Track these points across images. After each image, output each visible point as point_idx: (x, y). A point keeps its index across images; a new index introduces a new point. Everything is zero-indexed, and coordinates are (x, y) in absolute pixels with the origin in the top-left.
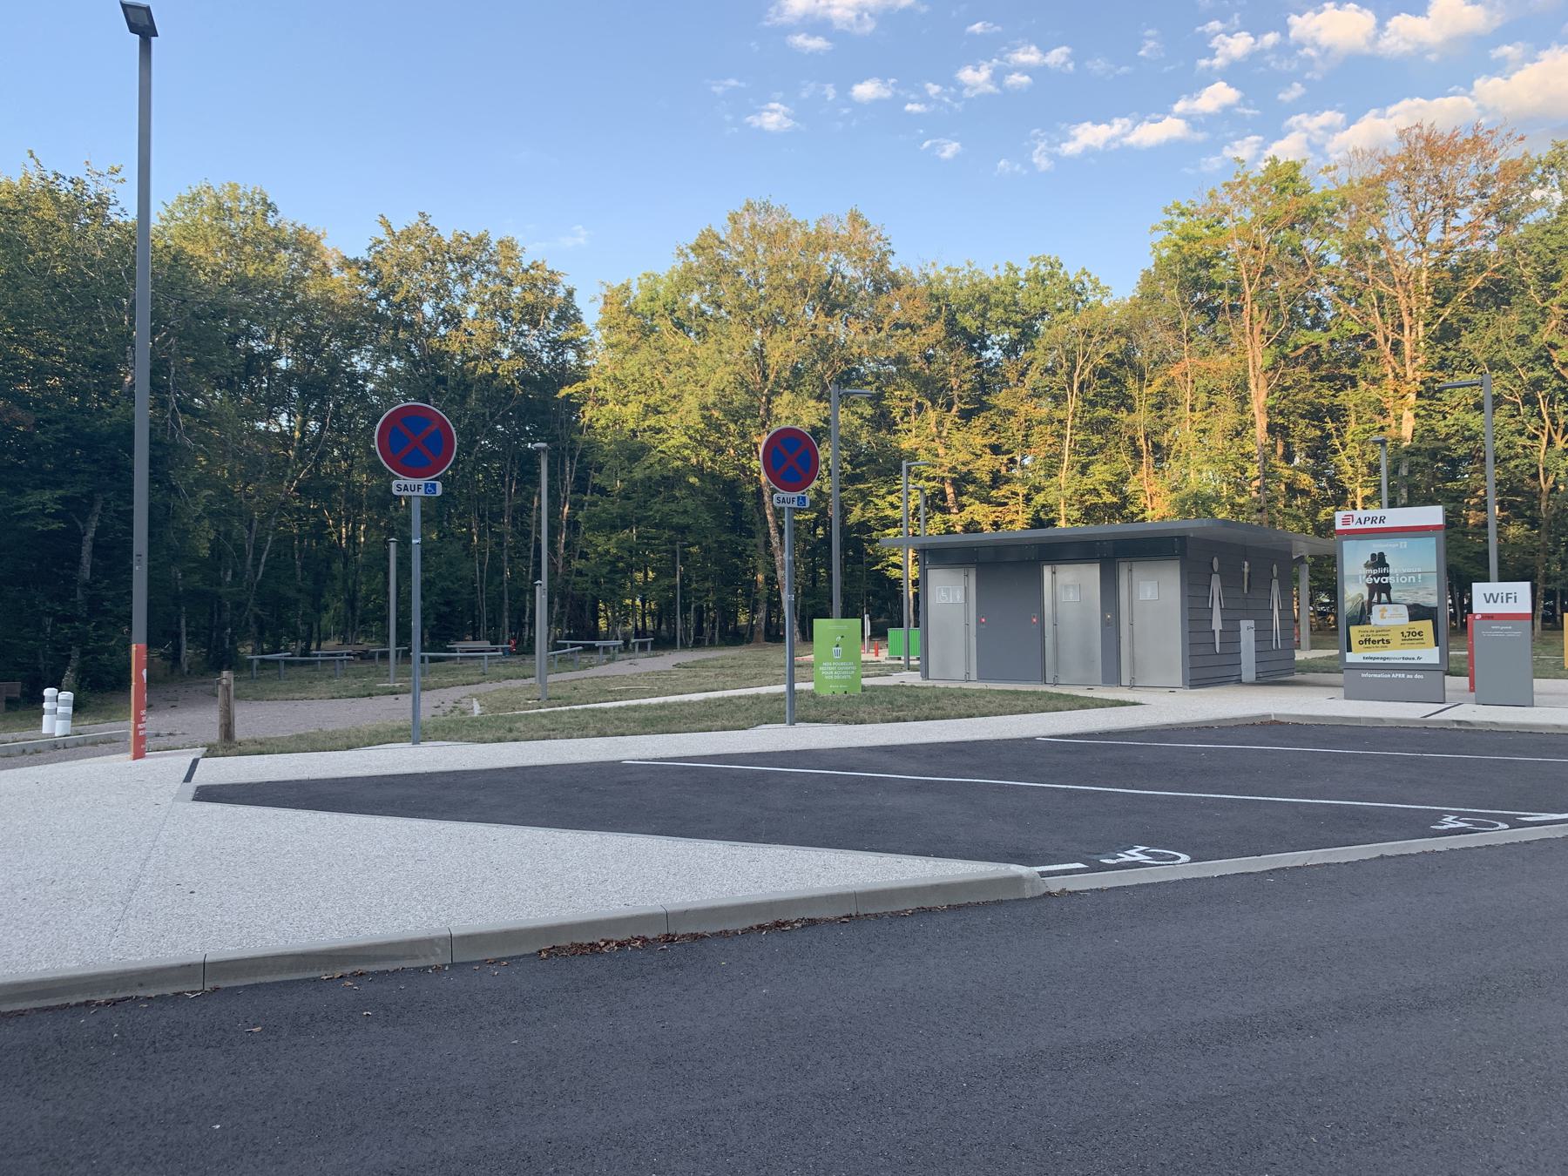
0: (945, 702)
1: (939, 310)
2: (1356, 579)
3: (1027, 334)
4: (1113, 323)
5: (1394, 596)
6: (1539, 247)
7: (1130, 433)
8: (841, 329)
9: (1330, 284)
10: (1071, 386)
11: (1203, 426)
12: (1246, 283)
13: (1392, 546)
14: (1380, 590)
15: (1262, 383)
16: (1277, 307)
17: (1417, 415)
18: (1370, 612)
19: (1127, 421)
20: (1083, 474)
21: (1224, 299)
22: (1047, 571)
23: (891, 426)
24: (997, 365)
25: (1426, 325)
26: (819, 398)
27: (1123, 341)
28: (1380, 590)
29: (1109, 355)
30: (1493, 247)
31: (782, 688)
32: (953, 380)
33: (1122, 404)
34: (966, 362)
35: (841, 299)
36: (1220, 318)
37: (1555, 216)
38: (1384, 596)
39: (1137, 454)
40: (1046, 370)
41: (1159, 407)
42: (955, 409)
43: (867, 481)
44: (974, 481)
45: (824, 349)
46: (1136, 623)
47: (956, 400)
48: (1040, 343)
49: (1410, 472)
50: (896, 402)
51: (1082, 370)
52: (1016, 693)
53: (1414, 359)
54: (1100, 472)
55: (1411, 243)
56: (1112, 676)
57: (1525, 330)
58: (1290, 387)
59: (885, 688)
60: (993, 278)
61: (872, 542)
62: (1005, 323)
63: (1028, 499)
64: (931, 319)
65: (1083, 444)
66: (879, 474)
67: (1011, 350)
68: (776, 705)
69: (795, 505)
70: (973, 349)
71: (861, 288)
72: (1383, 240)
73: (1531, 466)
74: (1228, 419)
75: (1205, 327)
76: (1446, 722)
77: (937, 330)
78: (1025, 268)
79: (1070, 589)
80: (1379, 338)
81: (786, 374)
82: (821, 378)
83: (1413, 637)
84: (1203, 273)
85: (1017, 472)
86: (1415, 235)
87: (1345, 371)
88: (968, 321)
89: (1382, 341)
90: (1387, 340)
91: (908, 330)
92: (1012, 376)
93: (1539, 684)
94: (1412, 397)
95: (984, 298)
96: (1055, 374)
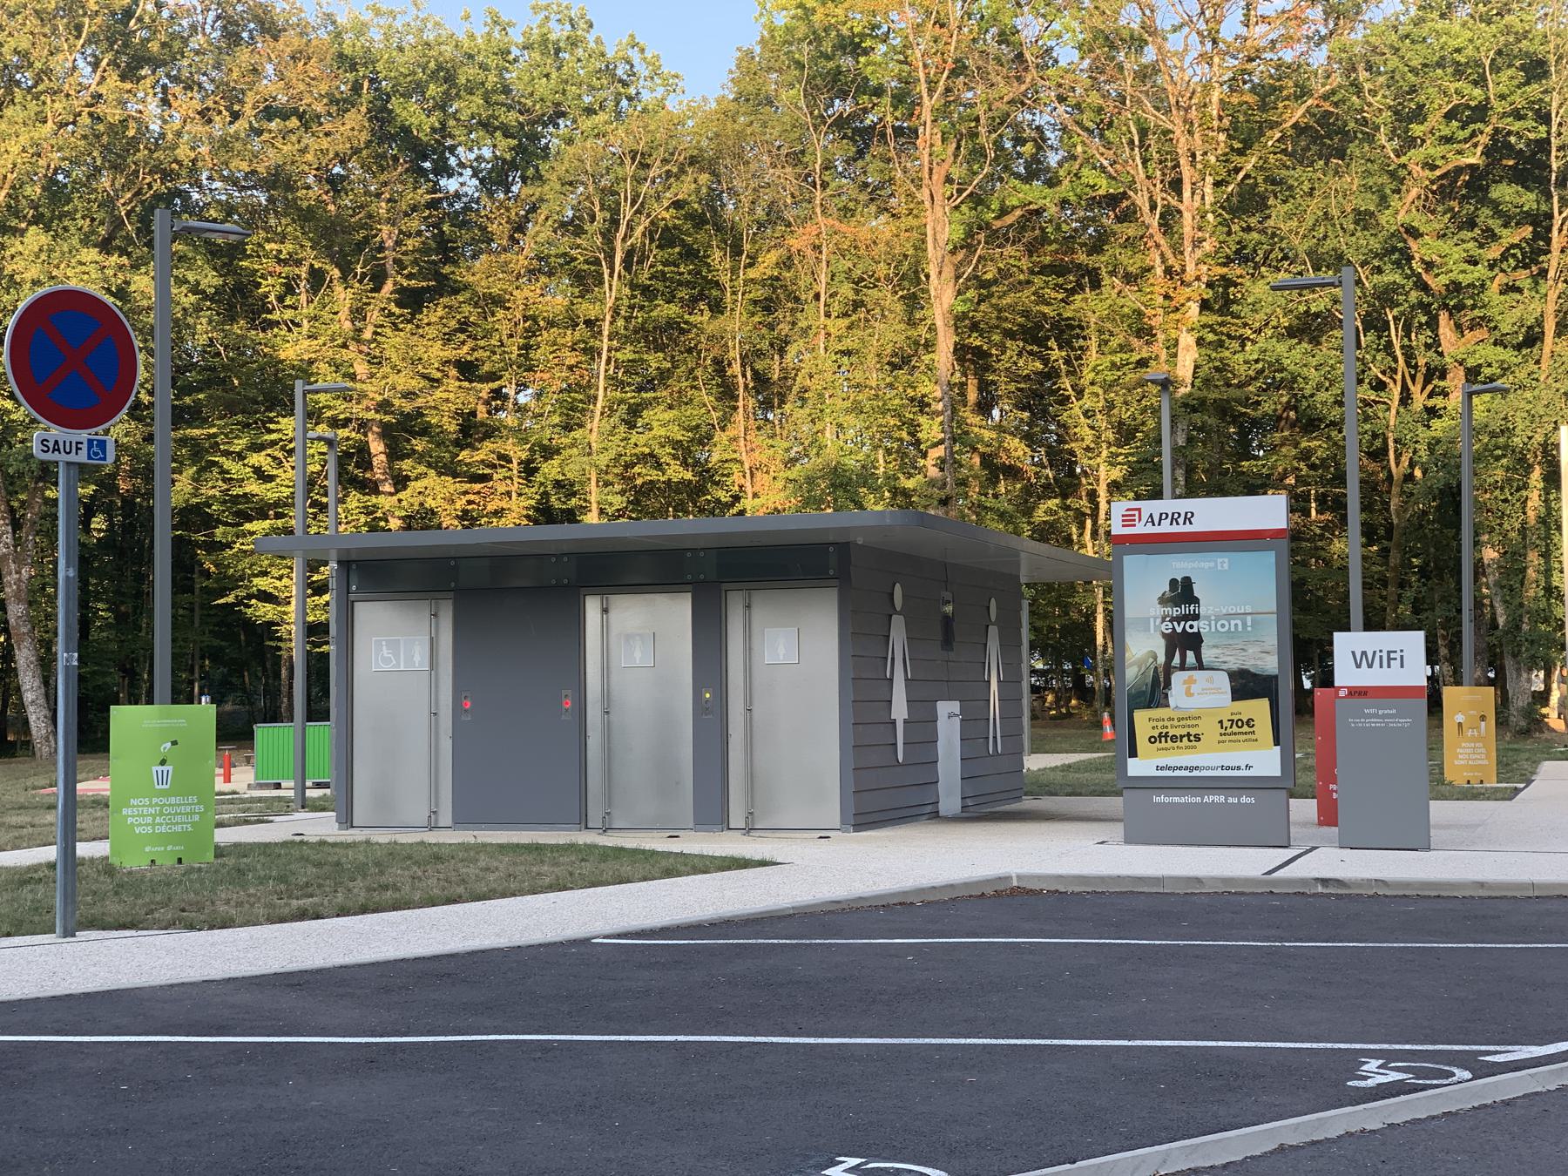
0: (395, 873)
1: (356, 88)
2: (1144, 623)
3: (526, 154)
4: (687, 143)
5: (1208, 654)
6: (1394, 62)
7: (715, 352)
8: (153, 107)
9: (1062, 99)
10: (610, 257)
11: (847, 344)
12: (923, 87)
13: (1198, 572)
14: (1185, 643)
15: (949, 272)
16: (973, 135)
17: (1200, 342)
18: (1168, 684)
19: (710, 328)
20: (631, 425)
21: (882, 113)
22: (592, 607)
23: (258, 314)
24: (467, 208)
25: (1217, 184)
26: (105, 246)
27: (704, 178)
28: (1185, 643)
29: (677, 205)
30: (1318, 58)
31: (50, 853)
32: (385, 229)
33: (701, 297)
34: (410, 197)
35: (154, 47)
36: (876, 149)
37: (1413, 11)
38: (1190, 655)
39: (727, 393)
40: (563, 225)
41: (768, 306)
42: (389, 286)
43: (204, 422)
44: (425, 431)
45: (117, 145)
46: (755, 708)
47: (391, 268)
48: (553, 172)
49: (1190, 440)
50: (269, 264)
51: (630, 228)
52: (537, 848)
53: (1197, 243)
54: (662, 423)
55: (1194, 38)
56: (712, 813)
57: (1368, 203)
58: (995, 282)
59: (265, 848)
60: (461, 36)
61: (214, 547)
62: (487, 126)
63: (529, 470)
64: (341, 105)
65: (631, 367)
66: (231, 409)
67: (495, 178)
68: (25, 892)
69: (82, 457)
70: (422, 172)
71: (193, 28)
72: (1150, 29)
73: (1375, 436)
74: (889, 333)
75: (848, 162)
76: (1304, 882)
77: (354, 126)
78: (523, 25)
79: (636, 645)
80: (1141, 200)
81: (34, 191)
82: (109, 203)
83: (1238, 728)
84: (847, 62)
85: (507, 418)
86: (1202, 26)
87: (1082, 258)
88: (414, 115)
89: (1146, 208)
90: (1153, 207)
91: (294, 122)
92: (499, 228)
93: (1440, 810)
94: (1194, 308)
95: (446, 74)
96: (579, 232)
